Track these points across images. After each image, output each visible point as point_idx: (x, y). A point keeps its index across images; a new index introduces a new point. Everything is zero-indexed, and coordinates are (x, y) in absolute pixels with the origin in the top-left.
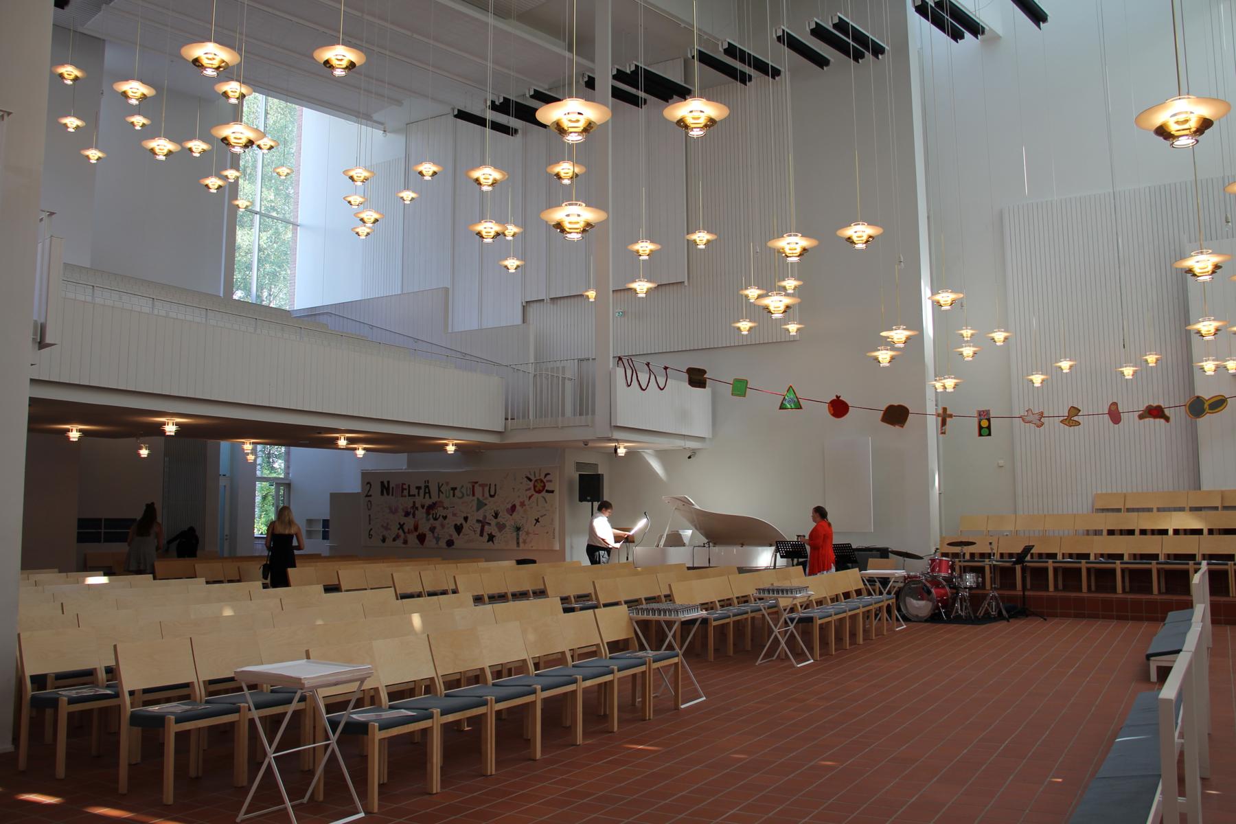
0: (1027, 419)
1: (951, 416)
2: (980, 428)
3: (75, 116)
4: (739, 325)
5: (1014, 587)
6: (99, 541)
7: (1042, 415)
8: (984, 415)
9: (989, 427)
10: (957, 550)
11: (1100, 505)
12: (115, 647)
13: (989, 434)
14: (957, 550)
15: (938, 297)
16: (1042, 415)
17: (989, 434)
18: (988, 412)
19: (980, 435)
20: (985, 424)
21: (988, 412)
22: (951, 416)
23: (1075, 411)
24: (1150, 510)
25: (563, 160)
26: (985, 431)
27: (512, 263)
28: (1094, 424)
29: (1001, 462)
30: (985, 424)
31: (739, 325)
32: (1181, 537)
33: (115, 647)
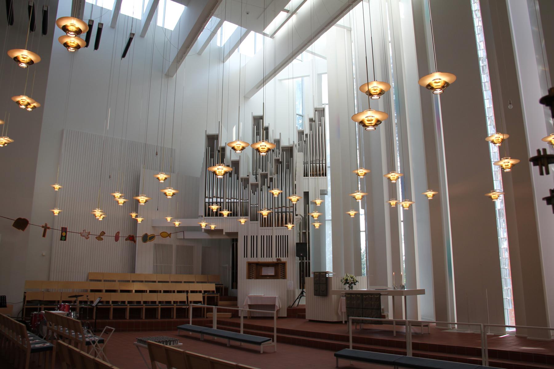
0: (83, 234)
1: (49, 228)
2: (62, 236)
3: (28, 49)
4: (54, 186)
5: (92, 319)
7: (89, 233)
8: (64, 230)
9: (65, 236)
11: (91, 277)
13: (65, 240)
16: (89, 233)
17: (65, 240)
18: (66, 229)
19: (61, 240)
20: (64, 234)
21: (66, 229)
22: (49, 228)
23: (103, 233)
24: (181, 282)
25: (24, 49)
26: (63, 238)
27: (169, 219)
28: (109, 240)
29: (44, 254)
30: (64, 234)
31: (54, 186)
32: (172, 289)
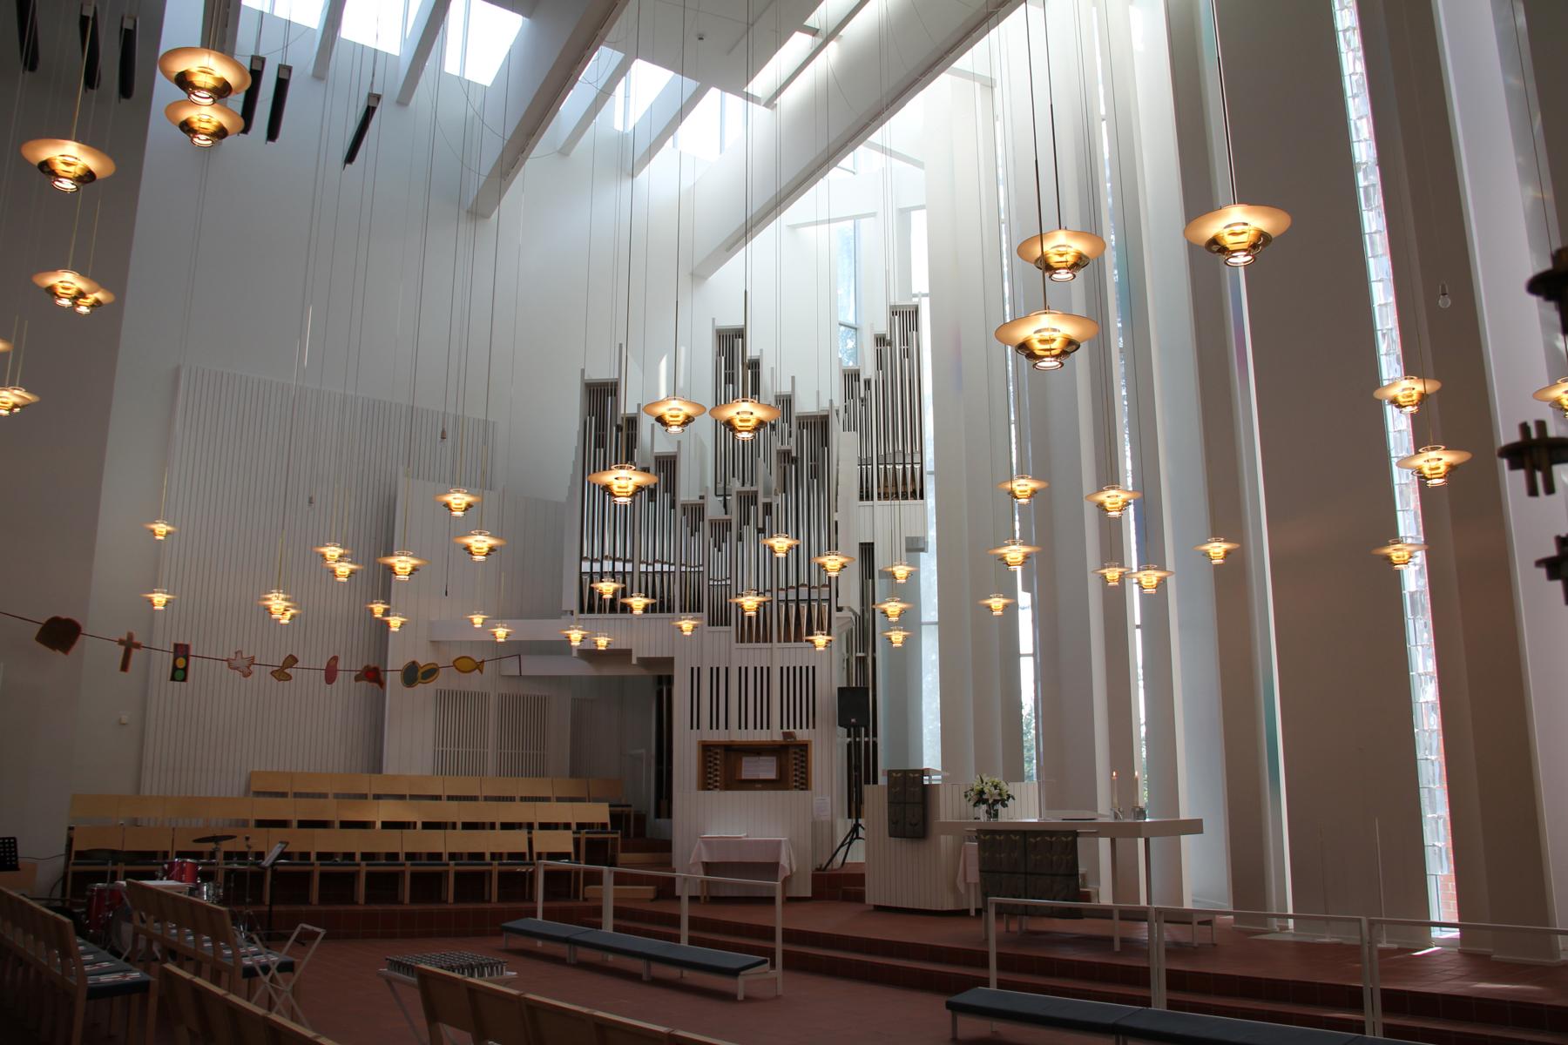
0: (235, 664)
1: (138, 646)
2: (175, 668)
5: (261, 902)
6: (767, 638)
7: (252, 661)
8: (182, 651)
9: (185, 669)
10: (210, 846)
11: (258, 786)
12: (351, 157)
13: (184, 680)
14: (210, 846)
15: (729, 413)
16: (252, 661)
17: (184, 680)
18: (187, 647)
19: (173, 679)
20: (181, 663)
21: (187, 647)
22: (138, 646)
23: (292, 660)
24: (512, 799)
26: (180, 674)
28: (307, 679)
29: (125, 719)
30: (181, 663)
33: (351, 157)
